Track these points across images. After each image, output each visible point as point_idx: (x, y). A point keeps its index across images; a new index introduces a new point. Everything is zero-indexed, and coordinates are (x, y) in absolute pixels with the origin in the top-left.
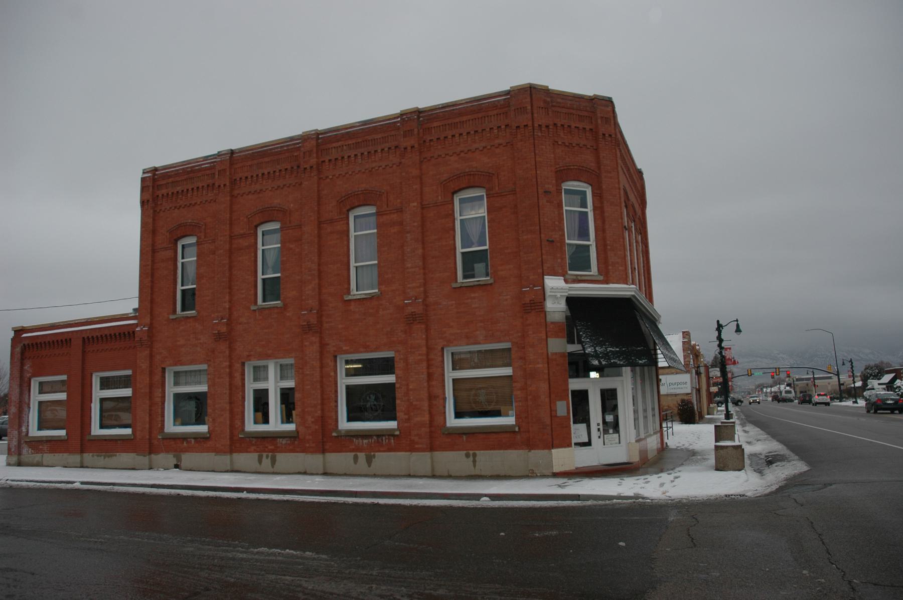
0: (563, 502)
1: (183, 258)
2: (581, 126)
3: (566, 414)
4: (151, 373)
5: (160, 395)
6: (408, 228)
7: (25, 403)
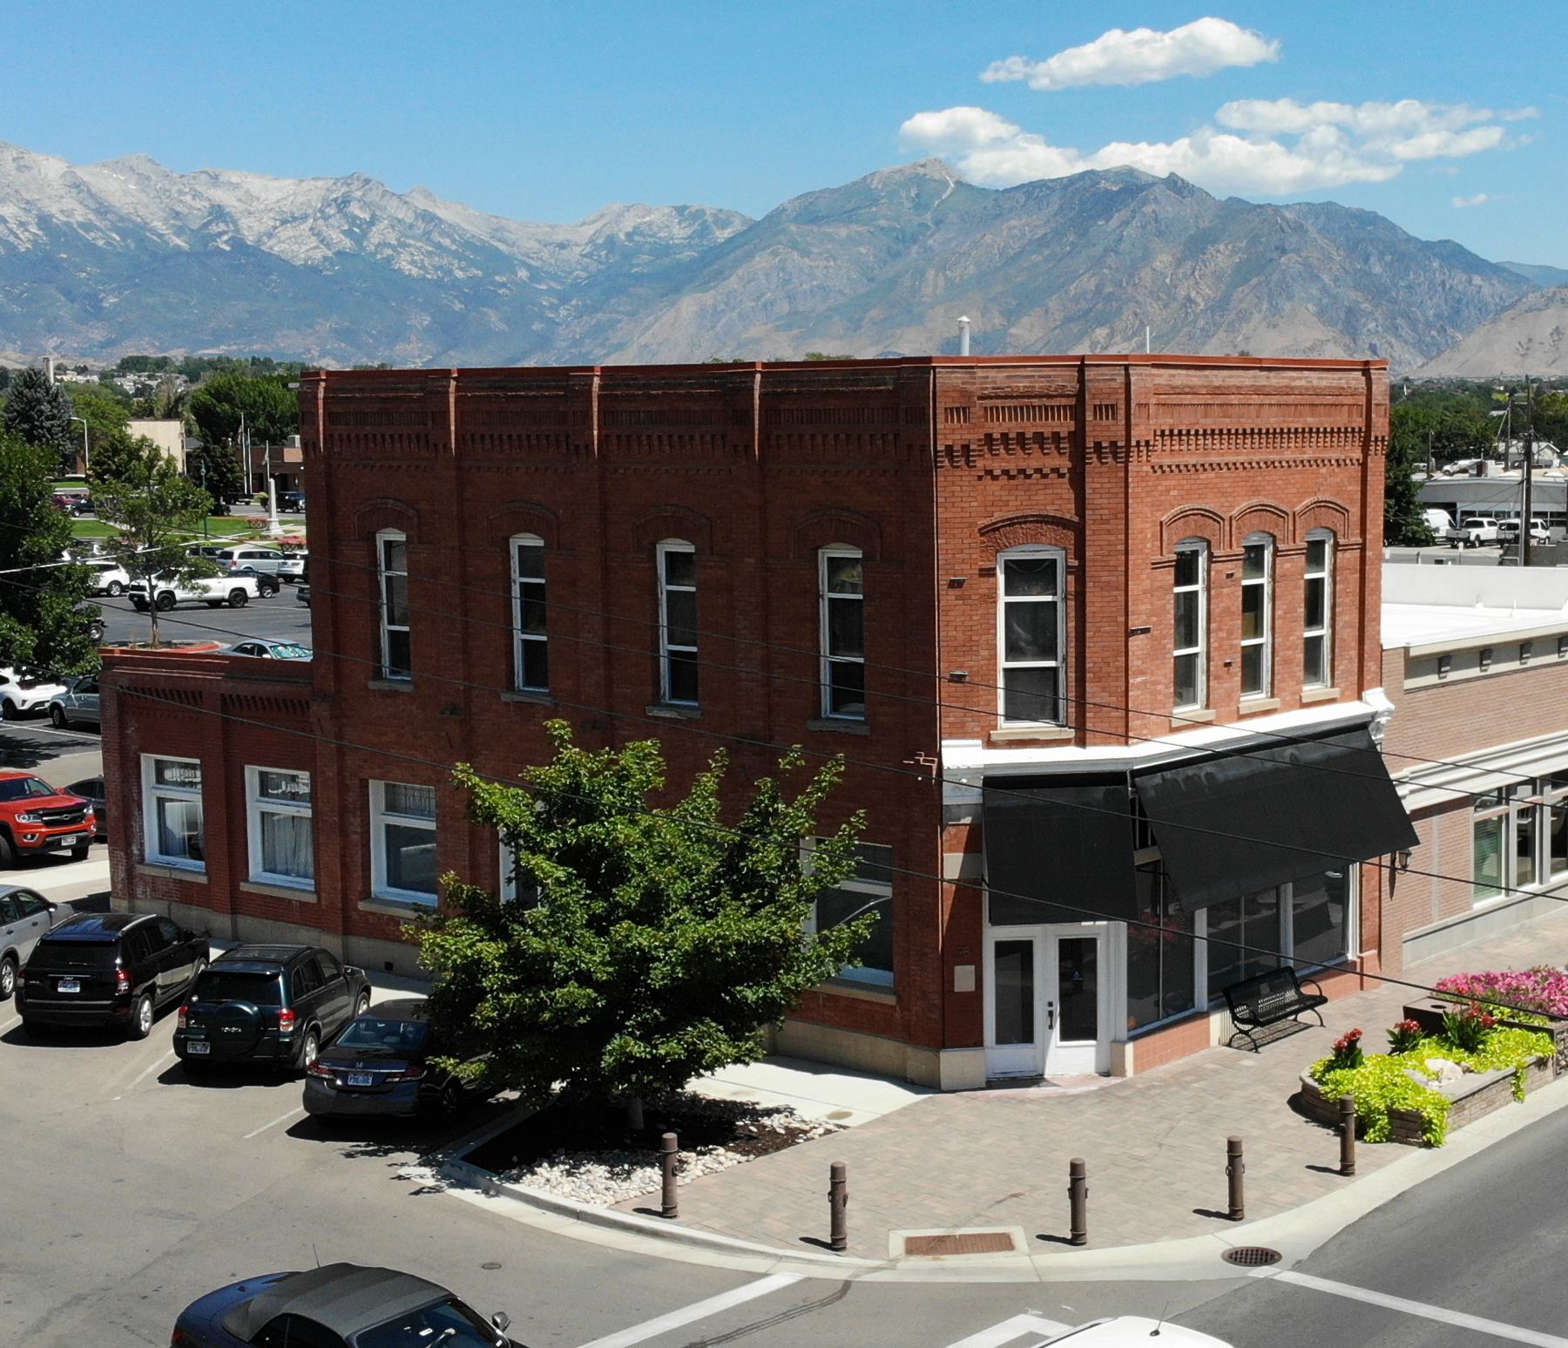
0: (1166, 1066)
1: (388, 567)
2: (1047, 432)
3: (972, 988)
4: (343, 789)
5: (359, 830)
6: (996, 321)
7: (134, 801)
